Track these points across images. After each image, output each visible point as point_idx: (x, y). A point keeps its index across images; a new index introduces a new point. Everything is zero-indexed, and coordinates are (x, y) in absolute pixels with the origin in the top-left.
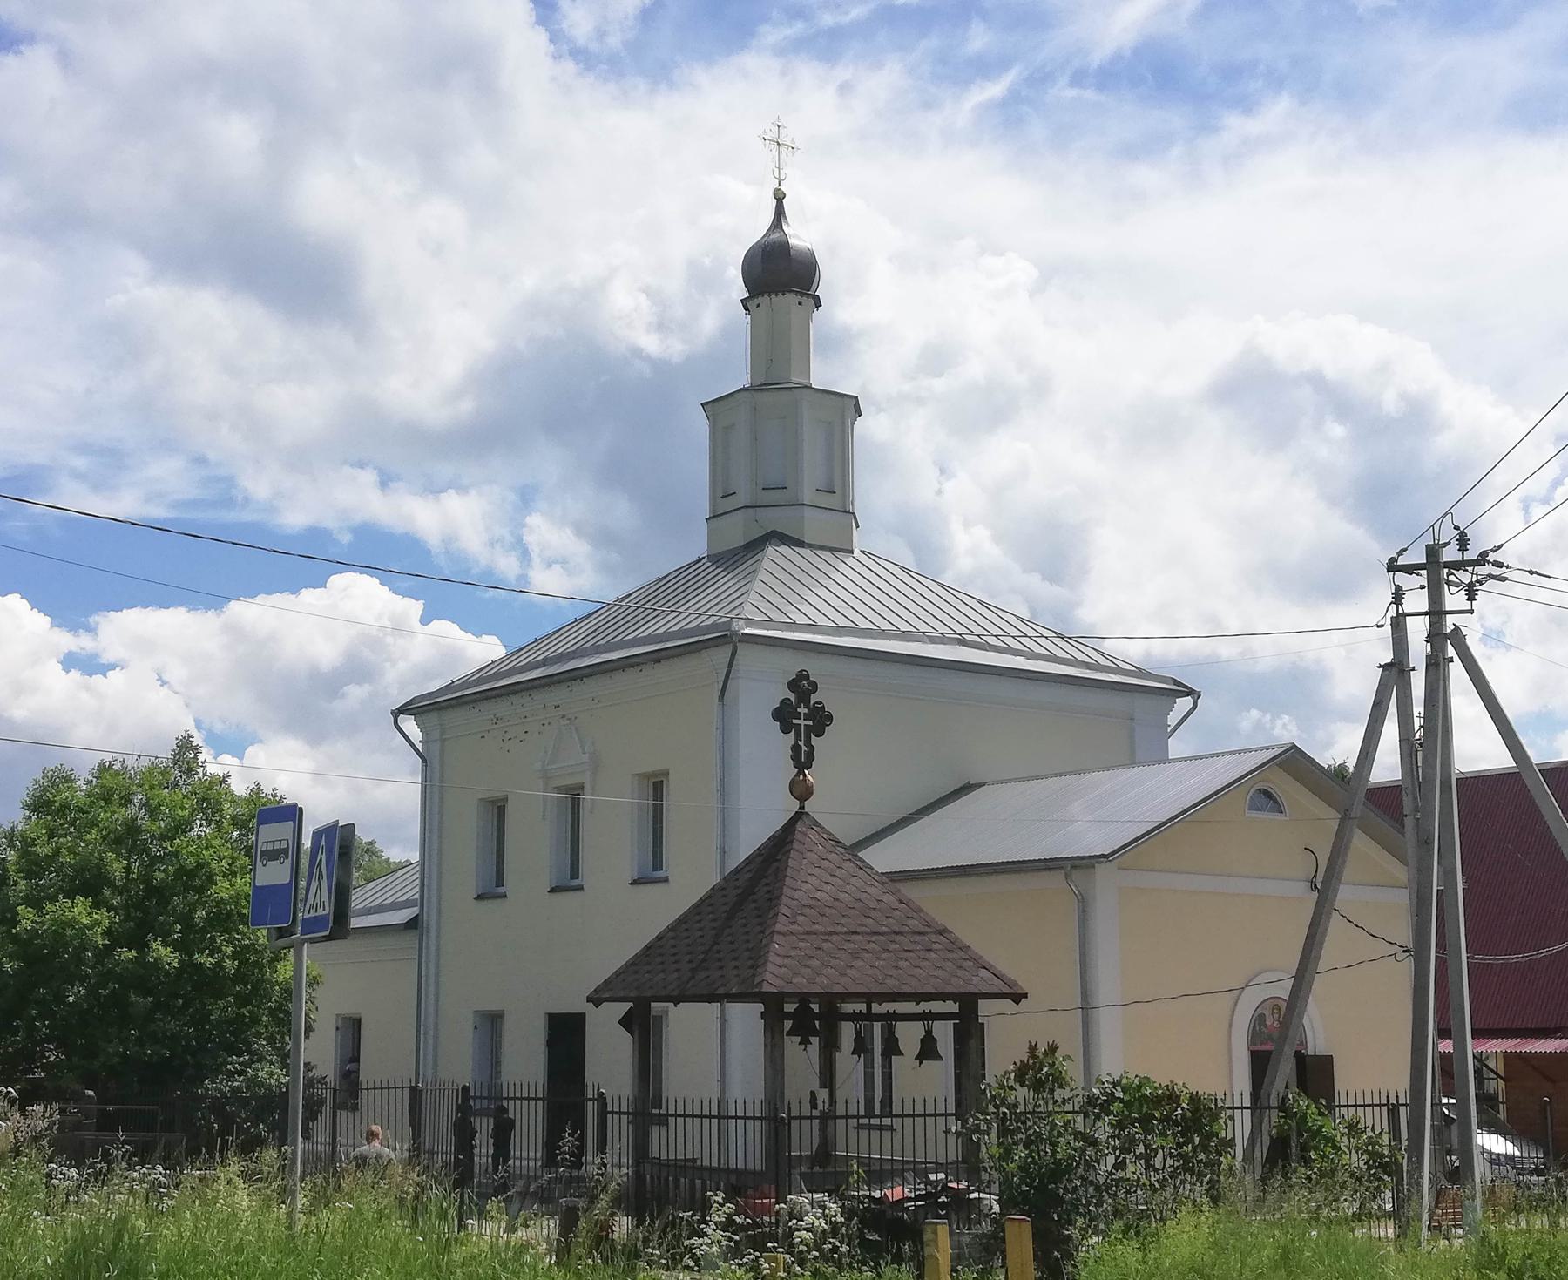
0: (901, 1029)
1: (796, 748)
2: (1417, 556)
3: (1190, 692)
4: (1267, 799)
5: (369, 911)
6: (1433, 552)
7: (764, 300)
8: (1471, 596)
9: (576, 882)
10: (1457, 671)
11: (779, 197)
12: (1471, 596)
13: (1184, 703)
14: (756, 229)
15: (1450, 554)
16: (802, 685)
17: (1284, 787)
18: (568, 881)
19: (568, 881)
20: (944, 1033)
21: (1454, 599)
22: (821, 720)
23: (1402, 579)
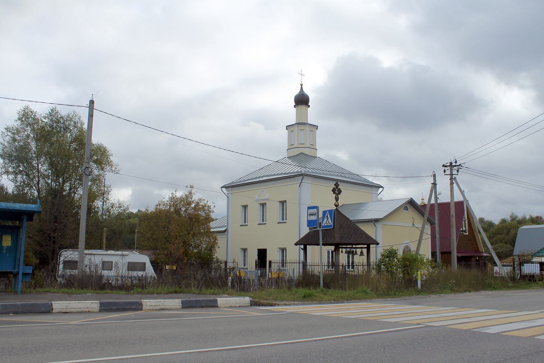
0: (357, 250)
1: (336, 197)
2: (449, 164)
3: (382, 187)
4: (406, 208)
5: (214, 228)
6: (451, 163)
7: (299, 107)
8: (458, 171)
9: (264, 222)
10: (455, 185)
11: (302, 85)
12: (458, 171)
13: (381, 189)
14: (297, 91)
15: (454, 164)
16: (337, 183)
17: (409, 207)
18: (263, 222)
19: (263, 222)
20: (365, 251)
21: (455, 172)
22: (340, 192)
23: (446, 168)
